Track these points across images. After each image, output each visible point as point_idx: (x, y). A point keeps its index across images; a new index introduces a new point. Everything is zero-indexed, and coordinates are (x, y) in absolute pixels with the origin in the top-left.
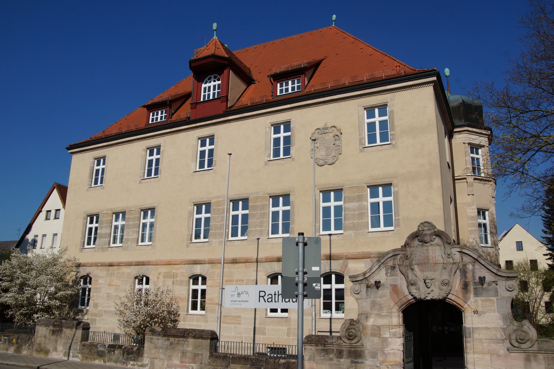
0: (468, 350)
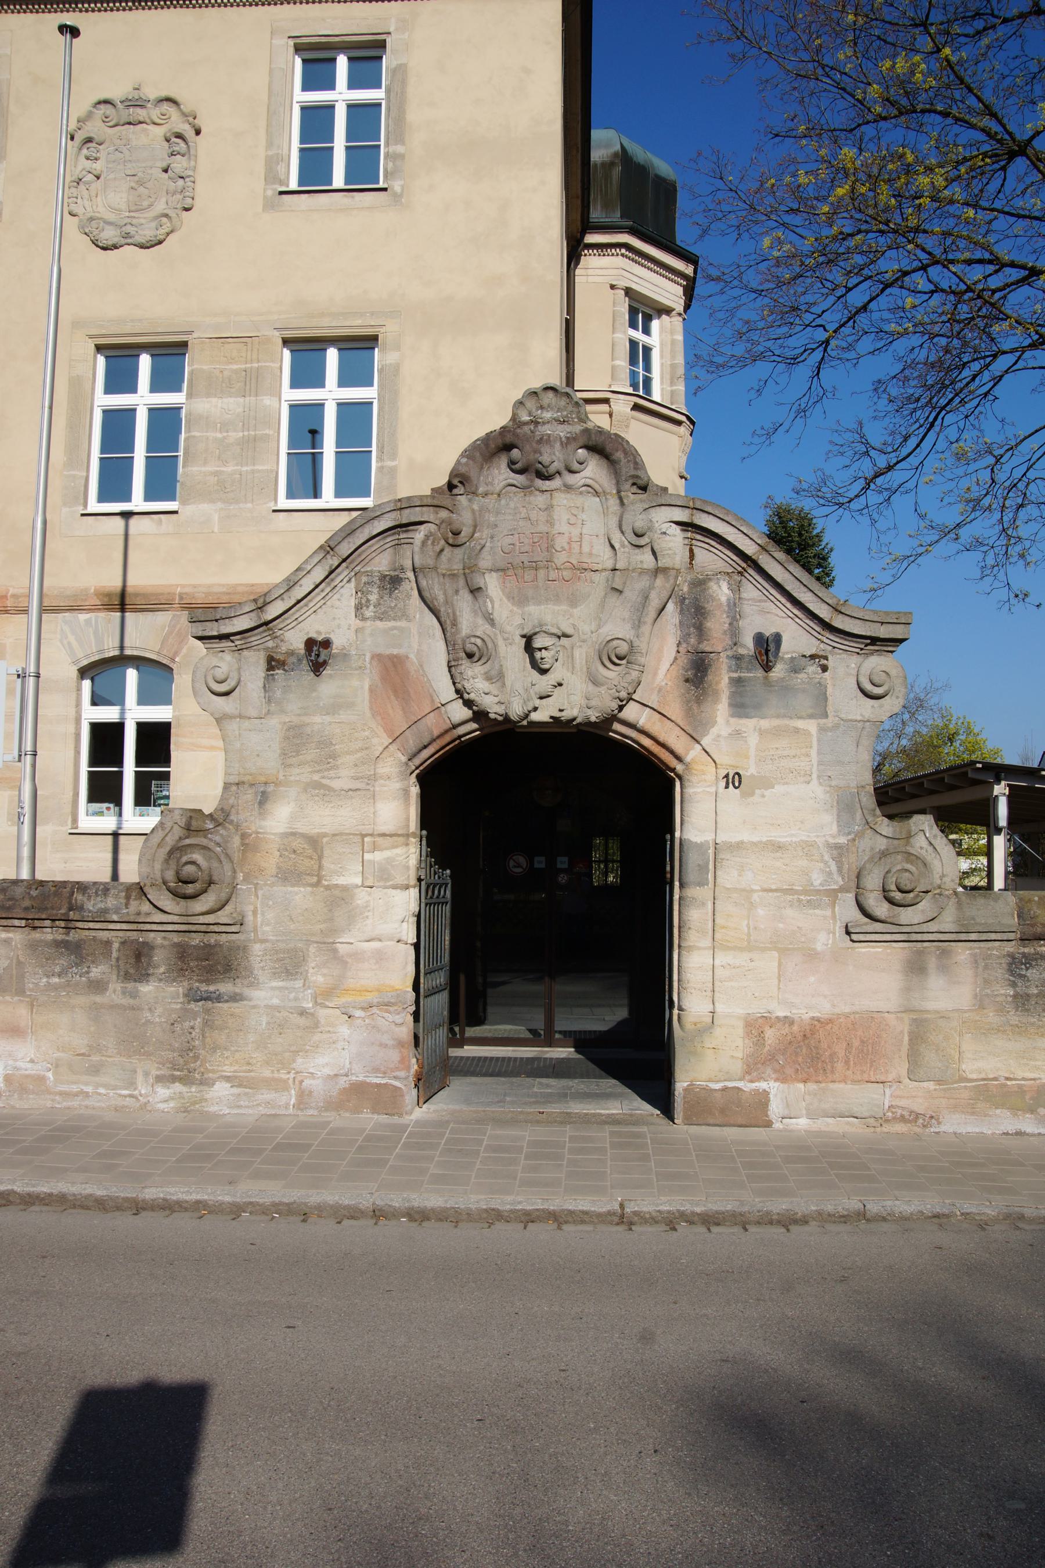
0: (692, 938)
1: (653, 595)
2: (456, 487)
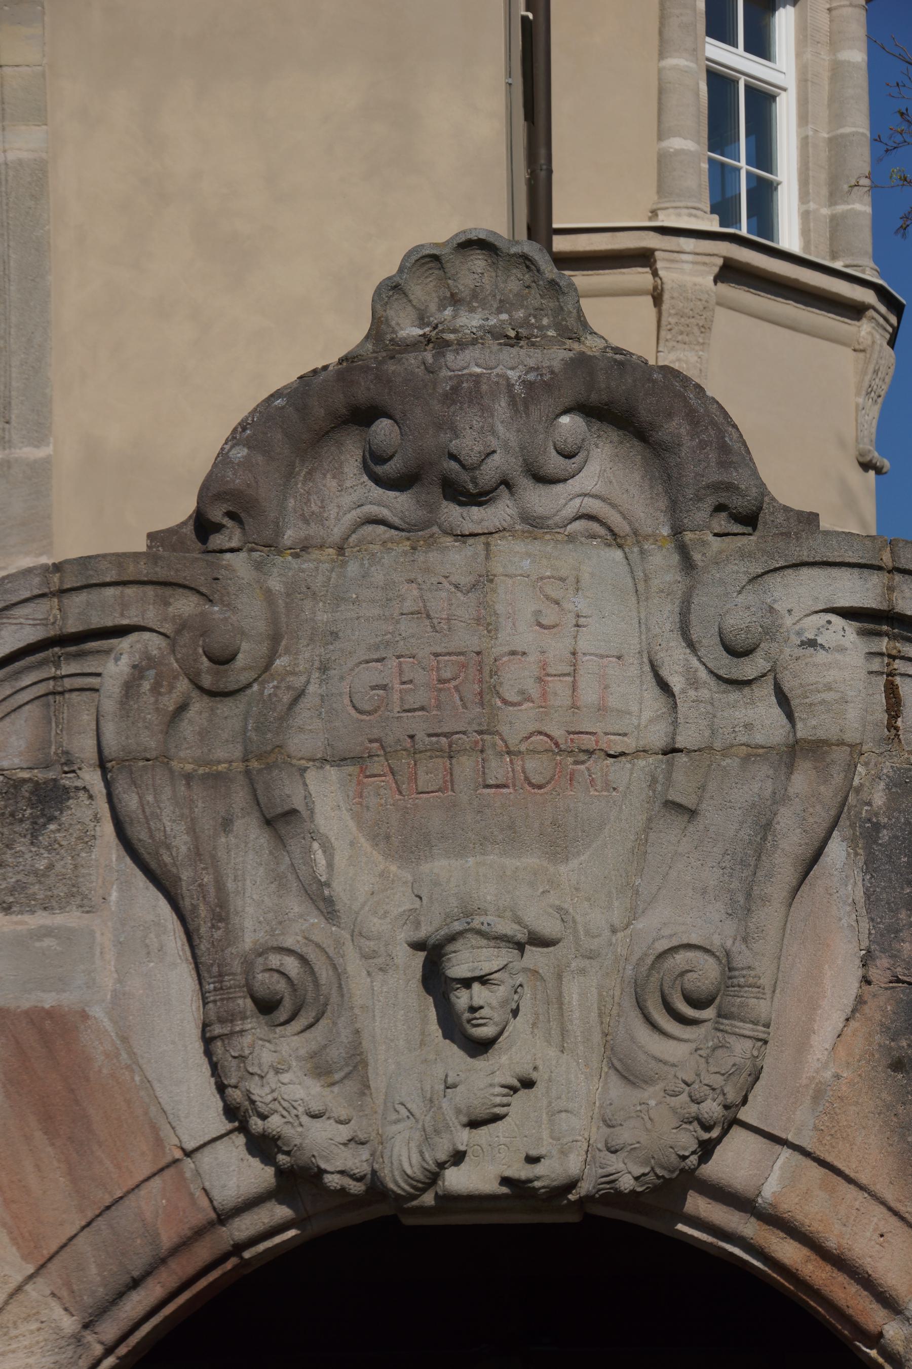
1: (786, 819)
2: (218, 528)
